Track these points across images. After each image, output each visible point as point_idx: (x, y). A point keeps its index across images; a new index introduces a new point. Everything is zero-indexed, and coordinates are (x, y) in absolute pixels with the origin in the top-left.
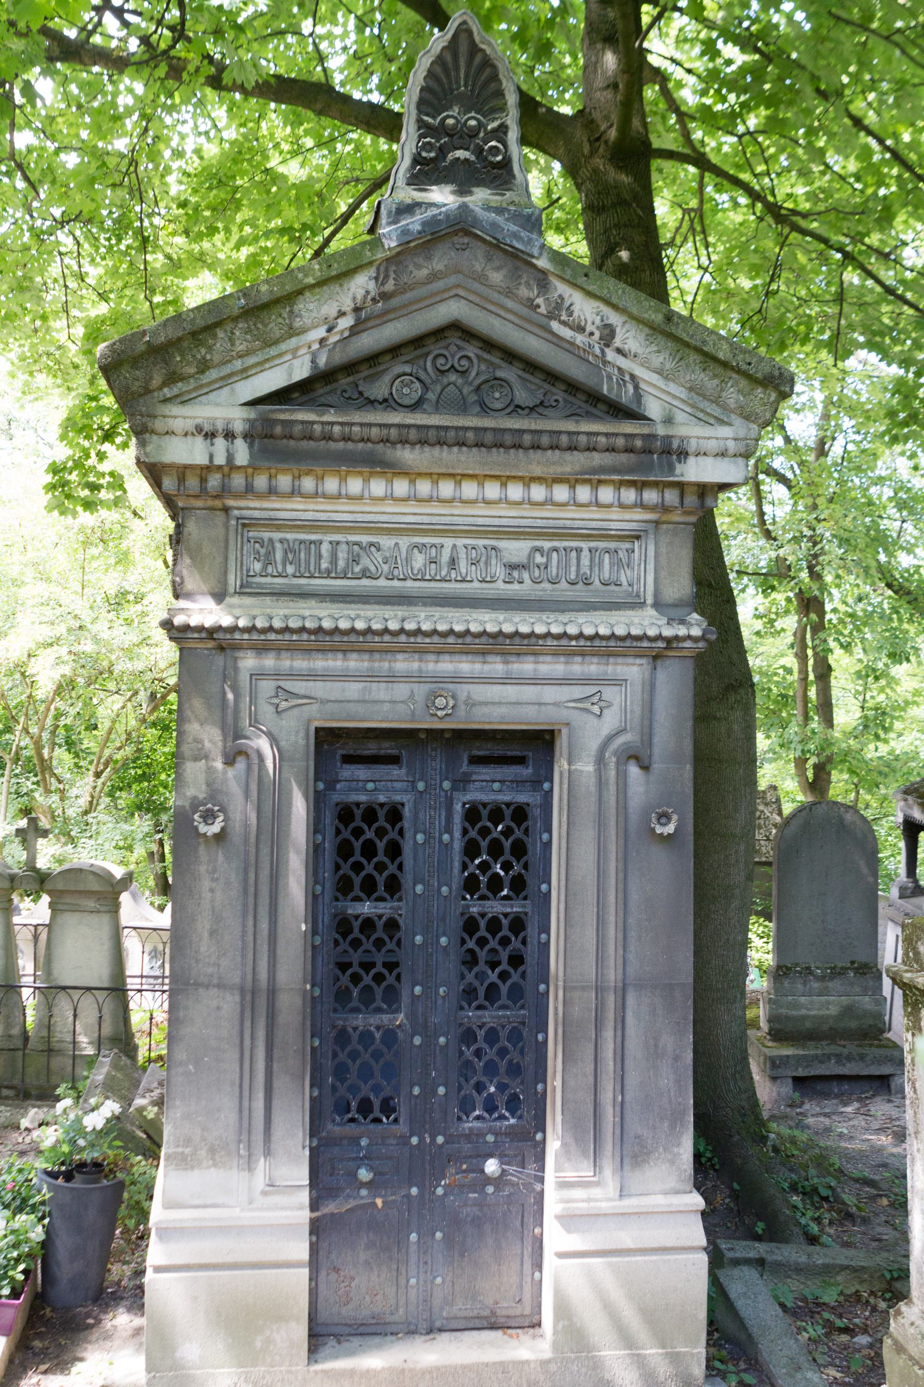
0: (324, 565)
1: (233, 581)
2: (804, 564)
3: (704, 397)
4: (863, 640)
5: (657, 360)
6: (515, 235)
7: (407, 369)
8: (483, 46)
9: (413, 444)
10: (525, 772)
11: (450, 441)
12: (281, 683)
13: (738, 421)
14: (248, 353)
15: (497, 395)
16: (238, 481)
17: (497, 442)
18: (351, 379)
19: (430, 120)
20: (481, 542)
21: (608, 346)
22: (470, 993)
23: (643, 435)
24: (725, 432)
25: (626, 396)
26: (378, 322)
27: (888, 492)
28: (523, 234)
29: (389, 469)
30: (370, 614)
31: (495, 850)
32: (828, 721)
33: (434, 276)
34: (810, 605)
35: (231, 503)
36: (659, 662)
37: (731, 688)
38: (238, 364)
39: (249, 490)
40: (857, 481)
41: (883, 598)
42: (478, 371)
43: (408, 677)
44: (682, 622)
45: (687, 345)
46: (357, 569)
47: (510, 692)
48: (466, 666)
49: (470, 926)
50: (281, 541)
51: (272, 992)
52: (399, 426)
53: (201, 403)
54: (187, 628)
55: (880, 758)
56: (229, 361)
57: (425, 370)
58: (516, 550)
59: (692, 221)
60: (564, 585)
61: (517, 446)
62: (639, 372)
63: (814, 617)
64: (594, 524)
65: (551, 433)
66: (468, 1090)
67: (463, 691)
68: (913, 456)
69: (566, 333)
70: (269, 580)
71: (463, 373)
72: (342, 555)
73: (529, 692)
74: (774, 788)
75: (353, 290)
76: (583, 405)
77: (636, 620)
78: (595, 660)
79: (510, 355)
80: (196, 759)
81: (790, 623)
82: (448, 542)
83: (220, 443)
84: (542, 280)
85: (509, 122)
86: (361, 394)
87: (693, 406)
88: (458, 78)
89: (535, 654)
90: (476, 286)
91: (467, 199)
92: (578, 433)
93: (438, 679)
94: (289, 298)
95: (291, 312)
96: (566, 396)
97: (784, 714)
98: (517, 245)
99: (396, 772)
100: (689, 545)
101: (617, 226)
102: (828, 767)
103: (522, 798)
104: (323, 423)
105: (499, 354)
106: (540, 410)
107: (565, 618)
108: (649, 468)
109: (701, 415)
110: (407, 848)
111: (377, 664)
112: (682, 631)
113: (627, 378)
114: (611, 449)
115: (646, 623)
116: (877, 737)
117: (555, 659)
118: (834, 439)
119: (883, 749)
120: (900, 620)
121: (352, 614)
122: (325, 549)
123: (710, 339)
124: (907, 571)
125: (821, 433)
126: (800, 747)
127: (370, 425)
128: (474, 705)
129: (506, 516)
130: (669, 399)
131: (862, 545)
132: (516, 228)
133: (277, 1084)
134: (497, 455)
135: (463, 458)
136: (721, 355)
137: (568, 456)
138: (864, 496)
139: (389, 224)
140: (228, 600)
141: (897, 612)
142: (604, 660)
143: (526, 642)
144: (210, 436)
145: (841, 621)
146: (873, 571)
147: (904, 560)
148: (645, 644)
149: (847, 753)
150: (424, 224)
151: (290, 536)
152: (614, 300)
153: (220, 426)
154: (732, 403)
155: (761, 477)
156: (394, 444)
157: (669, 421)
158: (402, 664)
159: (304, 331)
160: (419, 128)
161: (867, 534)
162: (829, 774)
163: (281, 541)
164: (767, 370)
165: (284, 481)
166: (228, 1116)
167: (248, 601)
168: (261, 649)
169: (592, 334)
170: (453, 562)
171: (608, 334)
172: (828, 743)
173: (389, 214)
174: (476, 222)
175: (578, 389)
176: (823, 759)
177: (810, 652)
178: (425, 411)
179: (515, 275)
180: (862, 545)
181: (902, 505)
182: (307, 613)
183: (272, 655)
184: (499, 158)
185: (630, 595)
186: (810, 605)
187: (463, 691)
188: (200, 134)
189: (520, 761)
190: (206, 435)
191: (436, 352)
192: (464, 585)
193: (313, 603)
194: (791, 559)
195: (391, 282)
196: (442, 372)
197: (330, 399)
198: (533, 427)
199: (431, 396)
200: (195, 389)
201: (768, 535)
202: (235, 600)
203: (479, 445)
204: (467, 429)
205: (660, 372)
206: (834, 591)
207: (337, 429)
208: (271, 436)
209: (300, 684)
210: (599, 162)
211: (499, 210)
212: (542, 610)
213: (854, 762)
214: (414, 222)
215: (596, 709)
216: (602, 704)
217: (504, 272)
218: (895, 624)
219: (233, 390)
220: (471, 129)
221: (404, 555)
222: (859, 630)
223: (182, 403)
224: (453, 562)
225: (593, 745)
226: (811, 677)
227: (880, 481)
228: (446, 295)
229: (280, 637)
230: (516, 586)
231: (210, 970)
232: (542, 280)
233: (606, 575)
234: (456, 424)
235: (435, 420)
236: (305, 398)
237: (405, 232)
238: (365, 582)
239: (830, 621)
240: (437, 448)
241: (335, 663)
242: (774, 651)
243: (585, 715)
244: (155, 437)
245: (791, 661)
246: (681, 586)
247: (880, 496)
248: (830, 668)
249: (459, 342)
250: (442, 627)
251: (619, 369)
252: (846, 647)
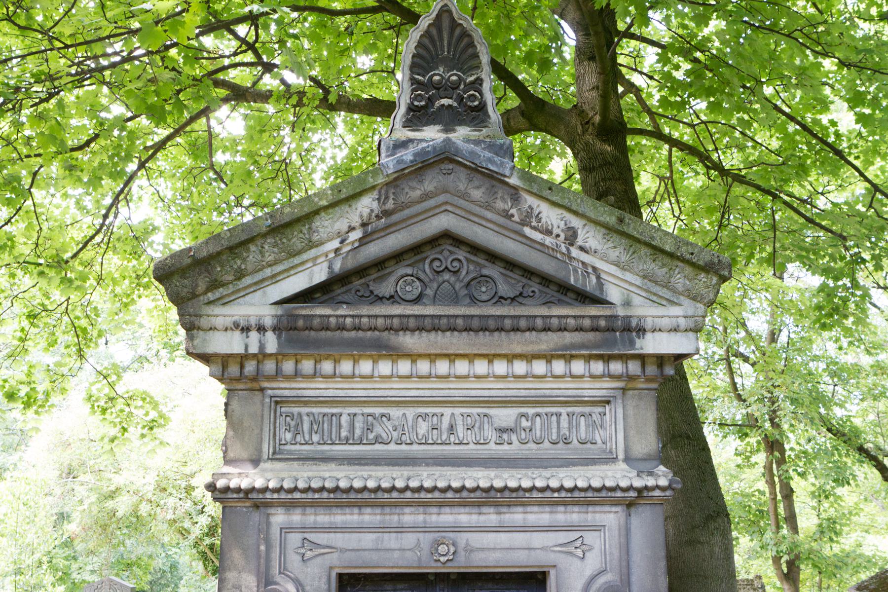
0: (344, 434)
1: (266, 449)
2: (767, 417)
3: (656, 282)
4: (814, 470)
5: (614, 254)
6: (490, 160)
7: (409, 271)
8: (460, 22)
9: (413, 331)
11: (444, 327)
12: (306, 535)
13: (686, 302)
14: (276, 262)
15: (484, 289)
16: (269, 366)
17: (484, 326)
18: (363, 281)
19: (420, 78)
20: (475, 411)
21: (572, 245)
23: (606, 317)
25: (590, 285)
26: (382, 234)
27: (822, 366)
28: (497, 159)
29: (396, 354)
30: (380, 474)
32: (794, 529)
33: (426, 196)
34: (774, 446)
35: (265, 384)
36: (633, 510)
37: (710, 518)
38: (268, 272)
39: (278, 374)
40: (799, 358)
41: (825, 440)
42: (468, 271)
43: (414, 528)
44: (651, 474)
45: (638, 241)
46: (371, 436)
47: (503, 539)
48: (464, 517)
50: (308, 415)
52: (400, 316)
53: (239, 304)
54: (227, 489)
55: (834, 555)
56: (261, 270)
57: (424, 271)
58: (505, 416)
59: (666, 185)
60: (546, 444)
61: (500, 329)
63: (777, 454)
64: (570, 393)
65: (528, 317)
67: (462, 539)
68: (837, 340)
69: (537, 236)
70: (298, 447)
71: (455, 272)
72: (359, 425)
73: (520, 539)
74: (760, 577)
75: (360, 209)
76: (555, 294)
77: (610, 474)
78: (576, 509)
79: (493, 257)
81: (761, 458)
82: (447, 411)
83: (254, 335)
84: (514, 194)
85: (483, 77)
86: (372, 292)
87: (647, 291)
88: (442, 46)
89: (523, 504)
91: (451, 136)
92: (551, 317)
95: (310, 228)
96: (541, 287)
97: (762, 524)
98: (492, 168)
100: (654, 408)
102: (797, 563)
104: (337, 316)
105: (483, 256)
106: (520, 299)
107: (547, 473)
108: (613, 343)
109: (654, 298)
111: (387, 517)
112: (651, 482)
113: (590, 270)
114: (579, 329)
115: (618, 475)
116: (831, 540)
117: (541, 509)
118: (780, 331)
119: (836, 548)
120: (840, 455)
121: (365, 474)
122: (344, 419)
123: (657, 235)
124: (841, 419)
125: (772, 327)
126: (775, 549)
127: (376, 316)
128: (472, 551)
129: (495, 389)
130: (627, 286)
131: (807, 403)
132: (490, 155)
134: (483, 338)
135: (455, 341)
136: (667, 248)
137: (543, 335)
138: (805, 369)
139: (388, 156)
140: (262, 465)
141: (837, 449)
142: (584, 509)
143: (514, 495)
144: (246, 330)
145: (797, 456)
146: (817, 421)
147: (838, 412)
148: (619, 494)
149: (811, 551)
150: (416, 155)
151: (315, 410)
152: (574, 207)
154: (680, 287)
155: (732, 358)
156: (397, 331)
157: (627, 304)
158: (409, 517)
159: (321, 243)
160: (412, 84)
161: (810, 395)
162: (798, 567)
163: (308, 415)
164: (708, 258)
165: (307, 366)
167: (278, 465)
168: (290, 505)
169: (558, 236)
170: (452, 428)
171: (571, 236)
172: (795, 545)
173: (388, 148)
174: (458, 152)
175: (550, 281)
176: (792, 557)
177: (776, 479)
178: (425, 305)
179: (492, 191)
180: (807, 403)
181: (833, 374)
182: (327, 475)
183: (298, 511)
184: (476, 103)
185: (604, 451)
186: (774, 446)
187: (462, 539)
188: (335, 147)
190: (242, 329)
191: (432, 257)
192: (462, 447)
193: (333, 466)
194: (757, 414)
195: (391, 202)
196: (438, 272)
197: (346, 298)
198: (512, 313)
199: (429, 292)
200: (233, 293)
201: (739, 397)
202: (268, 465)
203: (468, 329)
204: (457, 316)
205: (617, 264)
206: (791, 435)
207: (349, 321)
208: (295, 329)
209: (322, 535)
210: (589, 138)
211: (477, 142)
212: (528, 467)
213: (816, 559)
214: (407, 155)
215: (579, 552)
216: (584, 547)
217: (483, 190)
218: (836, 457)
219: (264, 293)
220: (453, 83)
221: (410, 423)
222: (810, 463)
223: (224, 304)
224: (452, 428)
226: (779, 497)
227: (816, 358)
228: (437, 211)
229: (304, 496)
230: (506, 447)
232: (514, 194)
233: (583, 436)
234: (447, 313)
235: (430, 310)
236: (326, 297)
237: (400, 161)
238: (378, 447)
239: (789, 456)
240: (433, 333)
241: (351, 517)
242: (753, 477)
243: (570, 558)
244: (201, 333)
245: (762, 485)
246: (647, 442)
247: (816, 369)
248: (792, 490)
249: (451, 248)
250: (441, 484)
251: (583, 263)
252: (802, 475)
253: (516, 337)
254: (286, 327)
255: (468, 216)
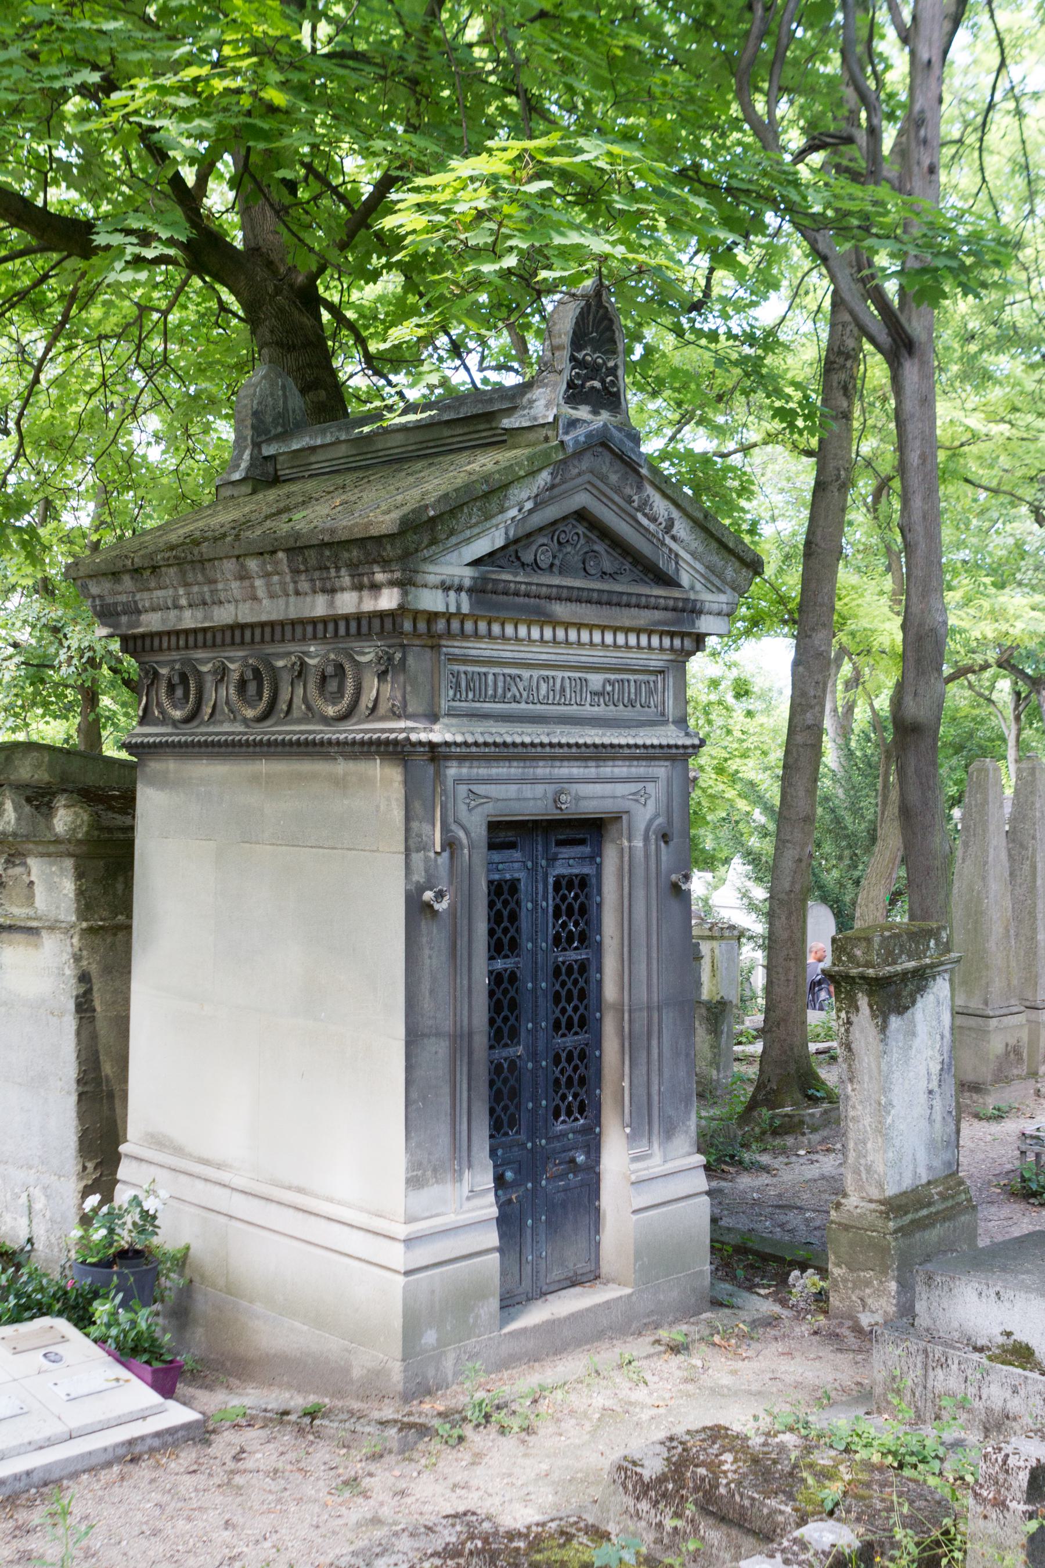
0: (490, 692)
5: (694, 545)
10: (586, 850)
13: (729, 591)
22: (557, 1026)
24: (723, 598)
31: (570, 913)
47: (598, 789)
48: (575, 770)
49: (557, 972)
51: (470, 1034)
58: (596, 680)
62: (682, 553)
66: (558, 1101)
69: (645, 522)
80: (418, 851)
82: (559, 674)
83: (452, 593)
90: (599, 483)
93: (560, 781)
94: (506, 486)
99: (517, 855)
101: (309, 365)
103: (586, 870)
110: (523, 914)
114: (666, 609)
122: (490, 677)
129: (596, 657)
133: (474, 1109)
134: (606, 611)
153: (457, 581)
158: (542, 770)
166: (444, 1140)
168: (462, 759)
170: (563, 689)
171: (670, 523)
179: (624, 478)
189: (582, 842)
212: (600, 726)
224: (563, 689)
225: (642, 826)
231: (430, 1022)
253: (626, 611)
254: (479, 590)
255: (601, 496)
